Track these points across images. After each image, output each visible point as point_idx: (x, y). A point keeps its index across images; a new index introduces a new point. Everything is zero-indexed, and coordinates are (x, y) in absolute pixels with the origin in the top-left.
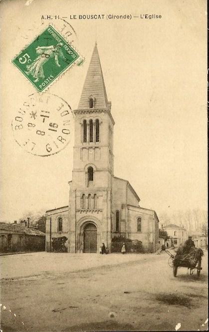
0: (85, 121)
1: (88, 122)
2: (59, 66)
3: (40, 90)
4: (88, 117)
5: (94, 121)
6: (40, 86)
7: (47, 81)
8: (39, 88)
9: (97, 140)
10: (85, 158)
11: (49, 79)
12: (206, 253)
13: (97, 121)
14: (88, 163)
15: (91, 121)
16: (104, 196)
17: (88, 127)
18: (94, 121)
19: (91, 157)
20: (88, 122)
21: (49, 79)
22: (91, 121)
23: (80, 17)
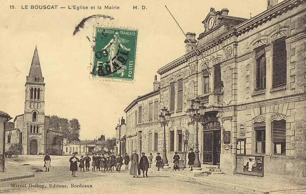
0: (32, 88)
1: (34, 89)
2: (129, 49)
3: (132, 78)
4: (34, 86)
5: (37, 89)
6: (129, 76)
7: (130, 68)
8: (130, 78)
9: (39, 98)
10: (32, 106)
11: (130, 66)
12: (78, 167)
13: (39, 89)
14: (34, 109)
15: (36, 89)
16: (43, 127)
17: (36, 128)
18: (37, 89)
19: (36, 107)
20: (34, 89)
21: (130, 66)
22: (36, 89)
23: (32, 7)
